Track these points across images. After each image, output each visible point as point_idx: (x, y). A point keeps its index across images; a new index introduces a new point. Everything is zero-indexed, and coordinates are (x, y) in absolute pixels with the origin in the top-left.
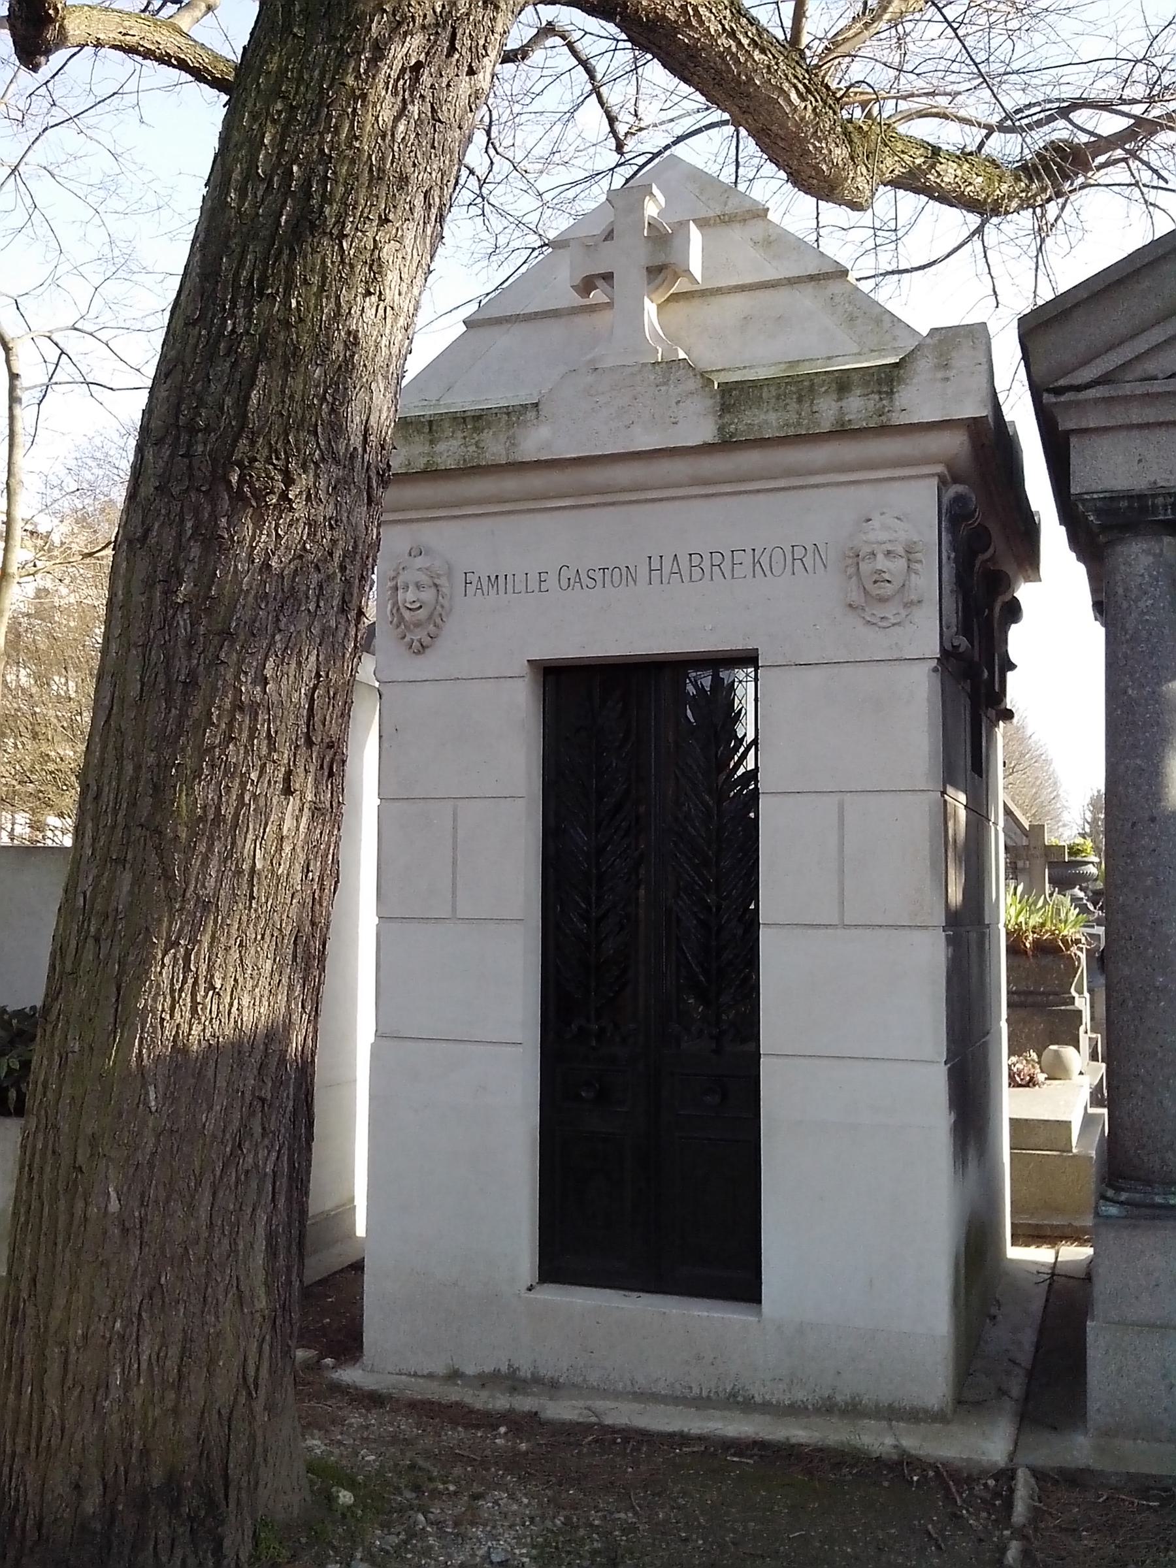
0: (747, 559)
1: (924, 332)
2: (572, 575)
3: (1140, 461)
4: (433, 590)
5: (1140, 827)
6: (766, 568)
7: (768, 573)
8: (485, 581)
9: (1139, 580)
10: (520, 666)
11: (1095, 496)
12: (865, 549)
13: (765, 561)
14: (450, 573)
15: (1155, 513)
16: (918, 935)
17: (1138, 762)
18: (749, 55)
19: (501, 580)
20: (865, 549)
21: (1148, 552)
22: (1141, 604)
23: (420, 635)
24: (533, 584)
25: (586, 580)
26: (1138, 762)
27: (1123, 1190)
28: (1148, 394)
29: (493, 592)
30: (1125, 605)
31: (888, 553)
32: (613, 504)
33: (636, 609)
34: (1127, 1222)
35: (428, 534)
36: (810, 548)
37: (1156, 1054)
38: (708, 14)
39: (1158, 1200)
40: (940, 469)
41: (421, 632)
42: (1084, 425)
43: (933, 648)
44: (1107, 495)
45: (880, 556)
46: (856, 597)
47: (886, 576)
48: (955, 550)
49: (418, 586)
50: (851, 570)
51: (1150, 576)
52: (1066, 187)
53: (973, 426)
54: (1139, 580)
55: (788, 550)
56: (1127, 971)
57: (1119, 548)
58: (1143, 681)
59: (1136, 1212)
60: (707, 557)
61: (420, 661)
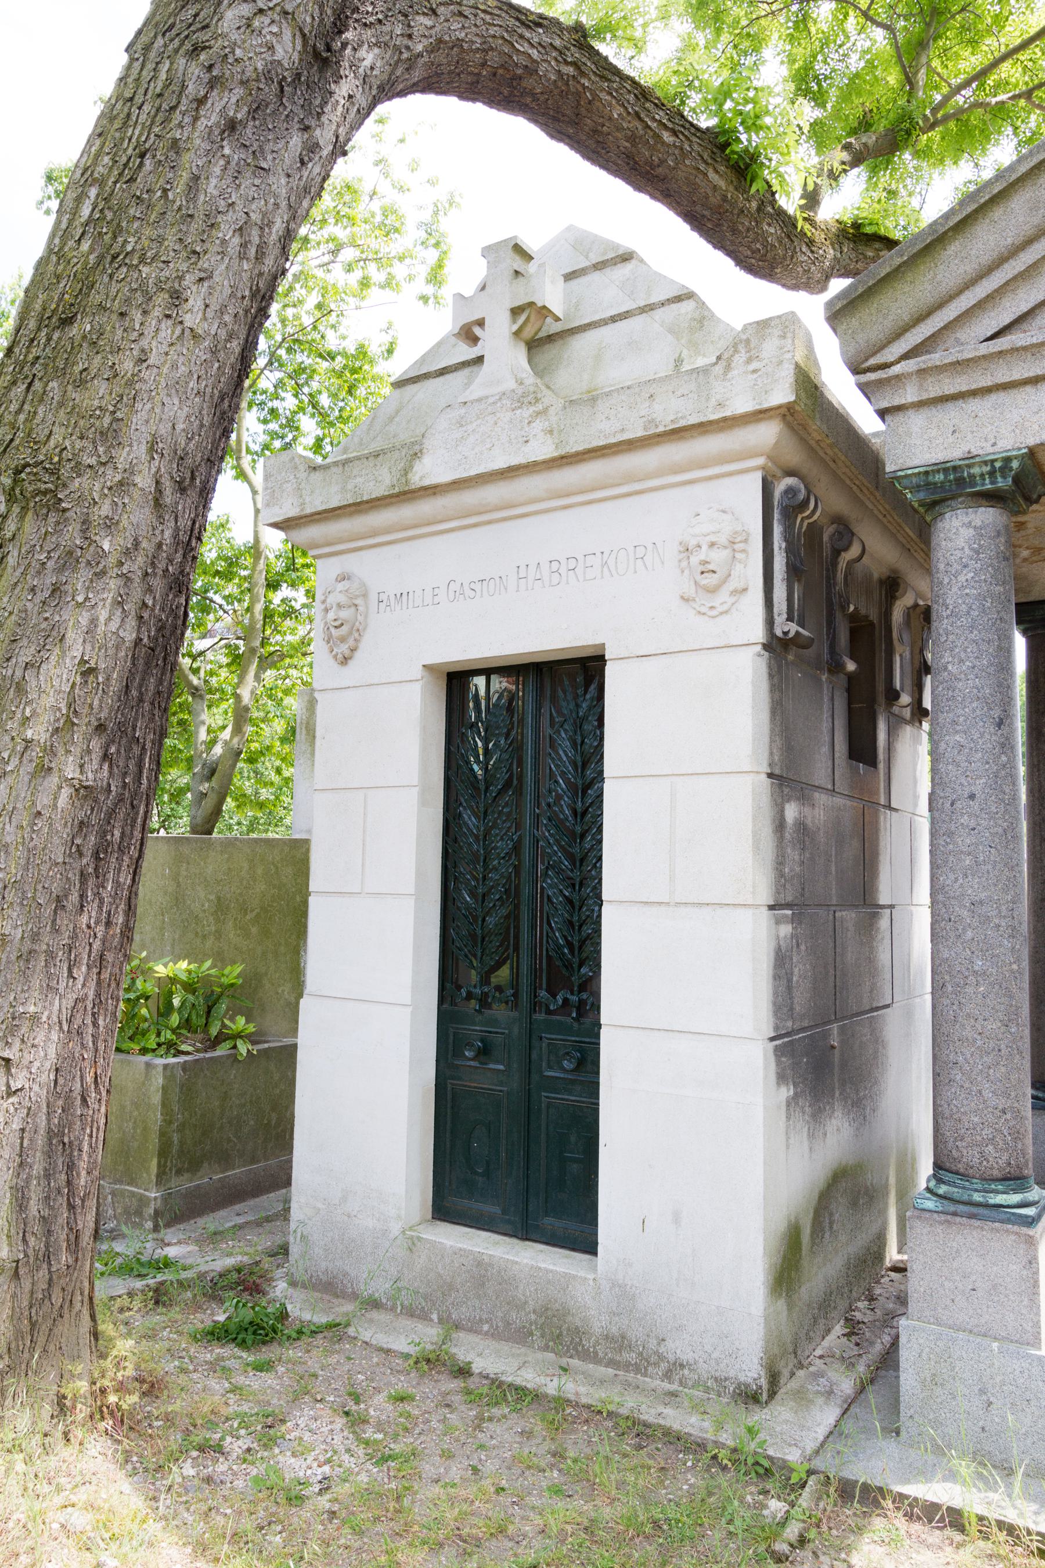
0: (596, 561)
1: (739, 328)
2: (458, 588)
3: (954, 432)
4: (353, 609)
5: (958, 805)
6: (613, 569)
7: (614, 572)
8: (392, 598)
9: (959, 554)
10: (417, 672)
11: (910, 472)
12: (693, 543)
13: (611, 562)
14: (365, 596)
15: (973, 484)
16: (749, 912)
17: (957, 738)
18: (657, 137)
19: (405, 596)
20: (693, 543)
21: (969, 525)
22: (962, 578)
23: (344, 648)
24: (428, 599)
25: (469, 593)
26: (957, 738)
27: (944, 1183)
28: (958, 362)
29: (398, 608)
30: (946, 580)
31: (712, 545)
32: (490, 522)
33: (513, 613)
34: (943, 1217)
35: (351, 563)
36: (650, 547)
37: (975, 1040)
38: (608, 98)
39: (977, 1197)
40: (761, 461)
41: (346, 645)
42: (897, 402)
43: (757, 633)
44: (921, 469)
45: (704, 547)
46: (690, 591)
47: (711, 567)
48: (786, 540)
49: (340, 606)
50: (684, 564)
51: (972, 549)
52: (638, 33)
53: (787, 413)
54: (959, 554)
55: (631, 549)
56: (946, 955)
57: (940, 525)
58: (963, 655)
59: (952, 1208)
60: (563, 562)
61: (346, 671)
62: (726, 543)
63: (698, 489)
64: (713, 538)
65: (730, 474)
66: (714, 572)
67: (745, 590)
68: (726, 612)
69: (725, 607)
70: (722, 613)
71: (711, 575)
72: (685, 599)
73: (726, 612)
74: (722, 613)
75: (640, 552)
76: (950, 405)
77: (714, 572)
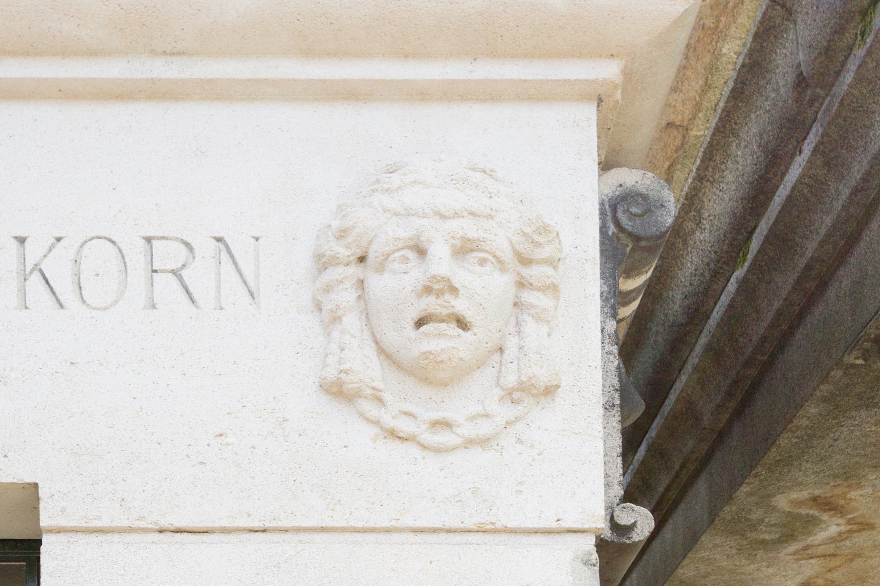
31: (464, 249)
36: (206, 247)
40: (609, 71)
47: (461, 306)
62: (507, 255)
63: (380, 121)
64: (471, 229)
65: (490, 94)
66: (462, 324)
67: (550, 391)
68: (483, 442)
69: (484, 428)
70: (469, 443)
71: (452, 329)
72: (338, 391)
73: (483, 442)
74: (469, 443)
75: (168, 255)
76: (550, 536)
77: (462, 324)
